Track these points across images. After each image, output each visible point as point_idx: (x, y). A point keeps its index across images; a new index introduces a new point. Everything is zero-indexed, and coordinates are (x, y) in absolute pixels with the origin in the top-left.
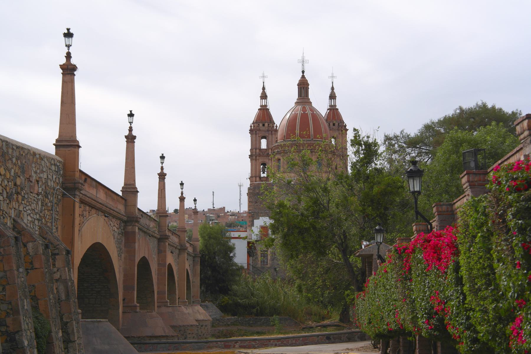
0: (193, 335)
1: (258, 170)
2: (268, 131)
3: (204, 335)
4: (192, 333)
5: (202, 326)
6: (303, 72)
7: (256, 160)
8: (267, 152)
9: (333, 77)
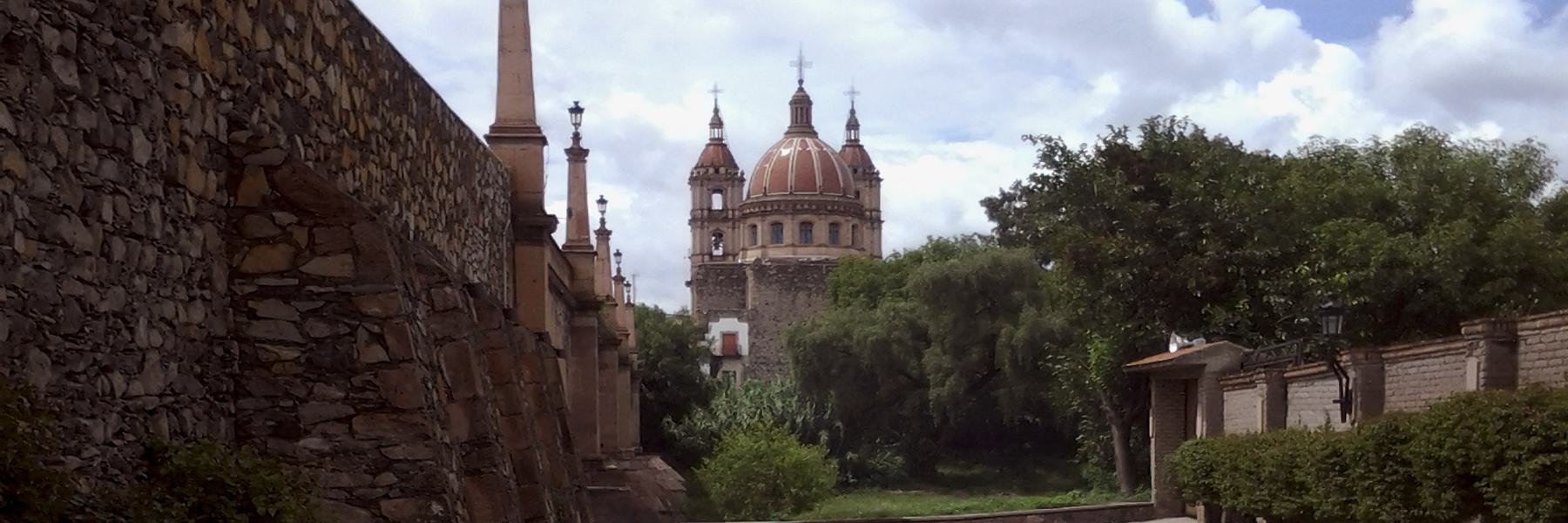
6: (801, 82)
9: (853, 92)
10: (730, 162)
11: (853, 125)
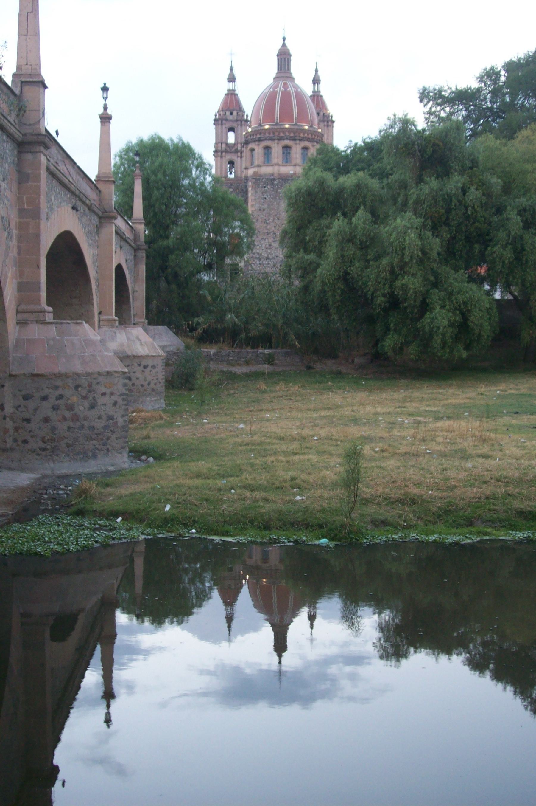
0: (114, 398)
1: (224, 169)
2: (237, 120)
3: (149, 384)
4: (112, 394)
5: (145, 367)
6: (284, 39)
7: (221, 157)
8: (236, 147)
10: (240, 109)
11: (316, 81)
